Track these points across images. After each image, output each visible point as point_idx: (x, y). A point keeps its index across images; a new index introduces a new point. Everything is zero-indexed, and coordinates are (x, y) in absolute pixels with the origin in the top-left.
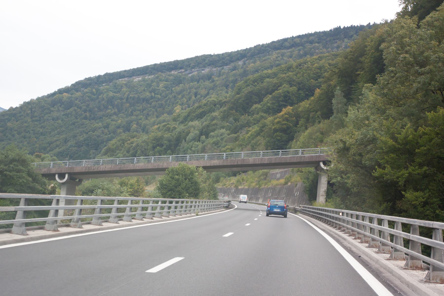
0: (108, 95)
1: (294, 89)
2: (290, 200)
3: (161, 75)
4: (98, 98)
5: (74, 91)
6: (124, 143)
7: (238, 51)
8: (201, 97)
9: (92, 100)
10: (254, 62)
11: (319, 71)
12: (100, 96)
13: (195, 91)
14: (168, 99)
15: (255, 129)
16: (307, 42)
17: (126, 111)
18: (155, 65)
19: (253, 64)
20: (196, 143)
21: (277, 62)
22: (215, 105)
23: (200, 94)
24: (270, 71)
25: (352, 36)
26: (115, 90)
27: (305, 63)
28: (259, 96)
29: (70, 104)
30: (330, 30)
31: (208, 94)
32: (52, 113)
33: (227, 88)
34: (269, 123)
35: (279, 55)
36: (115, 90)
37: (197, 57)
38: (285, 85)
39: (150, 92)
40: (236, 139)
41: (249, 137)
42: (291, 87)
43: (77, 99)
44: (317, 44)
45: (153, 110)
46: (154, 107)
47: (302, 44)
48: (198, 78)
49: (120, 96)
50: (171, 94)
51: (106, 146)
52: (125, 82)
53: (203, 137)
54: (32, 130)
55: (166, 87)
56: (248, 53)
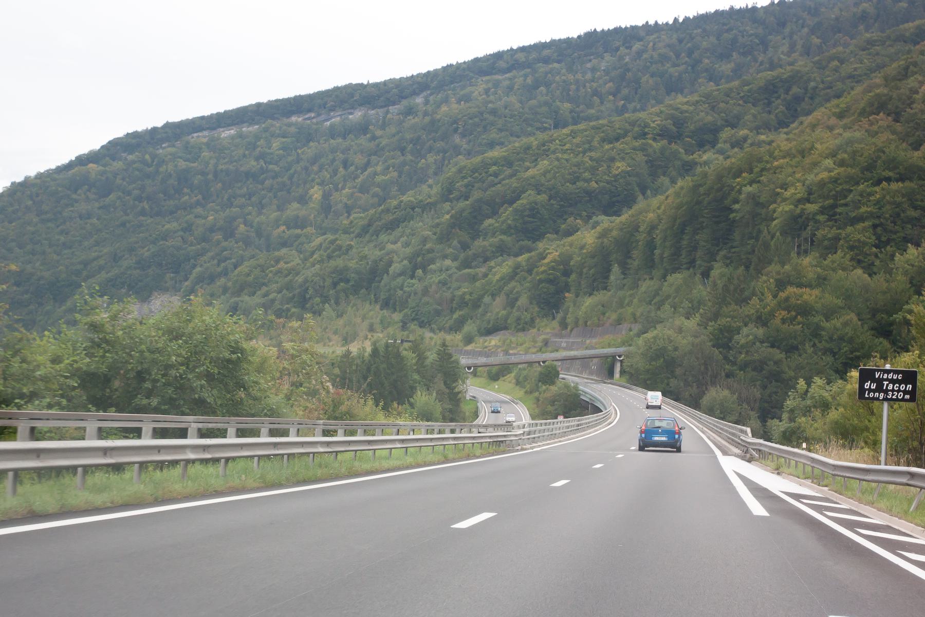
0: (176, 166)
1: (543, 198)
3: (272, 126)
5: (107, 158)
8: (357, 168)
11: (575, 169)
12: (161, 169)
18: (259, 105)
21: (490, 105)
22: (413, 209)
25: (617, 49)
26: (188, 156)
27: (552, 141)
30: (579, 37)
32: (76, 205)
34: (524, 264)
35: (490, 85)
36: (188, 156)
37: (336, 89)
38: (529, 192)
39: (257, 159)
41: (498, 281)
42: (539, 194)
44: (556, 65)
51: (194, 266)
52: (205, 140)
53: (419, 272)
55: (284, 148)
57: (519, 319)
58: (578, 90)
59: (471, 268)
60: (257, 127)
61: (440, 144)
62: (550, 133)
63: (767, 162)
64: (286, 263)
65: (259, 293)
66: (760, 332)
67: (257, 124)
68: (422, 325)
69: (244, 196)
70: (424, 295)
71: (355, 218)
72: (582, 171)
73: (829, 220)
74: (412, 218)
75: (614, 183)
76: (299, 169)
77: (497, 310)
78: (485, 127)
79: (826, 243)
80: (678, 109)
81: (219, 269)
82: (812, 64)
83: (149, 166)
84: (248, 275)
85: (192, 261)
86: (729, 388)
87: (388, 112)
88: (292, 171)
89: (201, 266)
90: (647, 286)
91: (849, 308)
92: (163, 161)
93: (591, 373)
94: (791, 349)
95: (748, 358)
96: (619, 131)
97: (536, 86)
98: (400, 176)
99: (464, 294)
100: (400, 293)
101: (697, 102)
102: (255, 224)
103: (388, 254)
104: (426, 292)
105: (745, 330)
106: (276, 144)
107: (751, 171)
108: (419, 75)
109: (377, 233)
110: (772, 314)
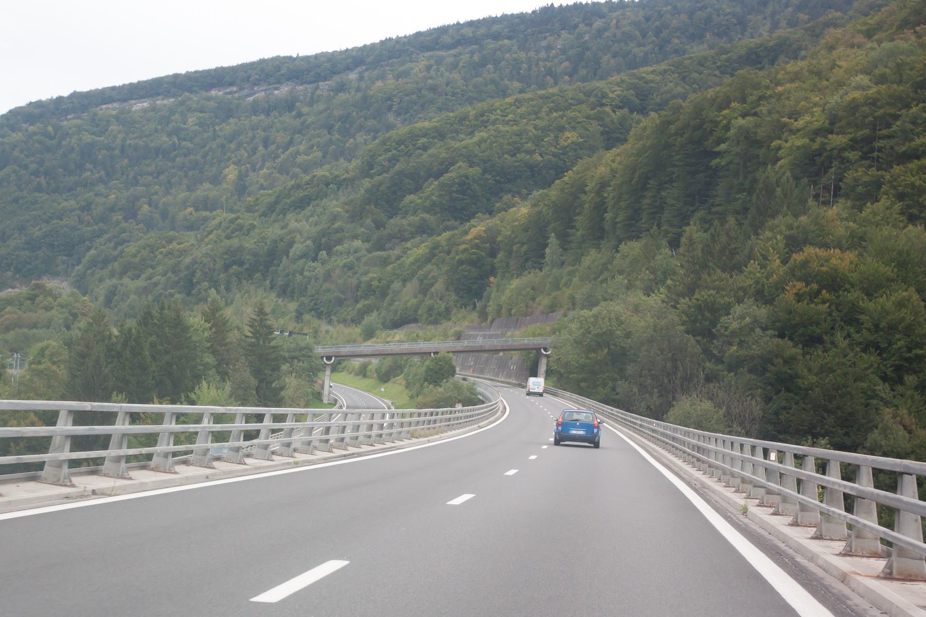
0: (80, 140)
1: (475, 171)
3: (189, 99)
5: (6, 129)
7: (347, 50)
8: (278, 147)
10: (382, 77)
12: (64, 143)
15: (418, 249)
17: (123, 174)
18: (176, 76)
19: (379, 84)
20: (311, 264)
21: (430, 81)
22: (327, 185)
23: (273, 143)
25: (576, 27)
26: (95, 129)
27: (491, 111)
28: (416, 180)
30: (534, 12)
31: (291, 143)
33: (330, 134)
34: (444, 243)
35: (432, 62)
36: (95, 129)
37: (262, 61)
38: (460, 163)
39: (170, 135)
41: (412, 264)
42: (470, 167)
43: (15, 146)
44: (506, 42)
47: (475, 41)
49: (106, 142)
50: (215, 140)
51: (89, 249)
52: (114, 113)
53: (323, 254)
55: (201, 124)
57: (431, 309)
58: (530, 69)
59: (385, 250)
61: (371, 123)
63: (767, 88)
64: (179, 244)
65: (143, 276)
66: (763, 312)
67: (173, 96)
68: (319, 316)
69: (151, 174)
70: (325, 281)
71: (262, 196)
73: (862, 158)
74: (326, 196)
75: (562, 157)
76: (215, 146)
77: (407, 298)
78: (423, 106)
79: (860, 189)
80: (641, 78)
81: (115, 253)
82: (803, 31)
83: (51, 138)
84: (135, 256)
85: (87, 243)
86: (711, 398)
87: (317, 88)
88: (207, 148)
90: (592, 258)
91: (904, 281)
92: (67, 134)
93: (509, 376)
94: (812, 341)
95: (743, 352)
96: (570, 101)
97: (483, 63)
98: (324, 157)
99: (372, 279)
100: (299, 278)
101: (665, 71)
102: (160, 205)
103: (290, 233)
104: (328, 276)
105: (738, 309)
106: (192, 120)
107: (743, 100)
108: (353, 49)
109: (284, 212)
110: (780, 287)
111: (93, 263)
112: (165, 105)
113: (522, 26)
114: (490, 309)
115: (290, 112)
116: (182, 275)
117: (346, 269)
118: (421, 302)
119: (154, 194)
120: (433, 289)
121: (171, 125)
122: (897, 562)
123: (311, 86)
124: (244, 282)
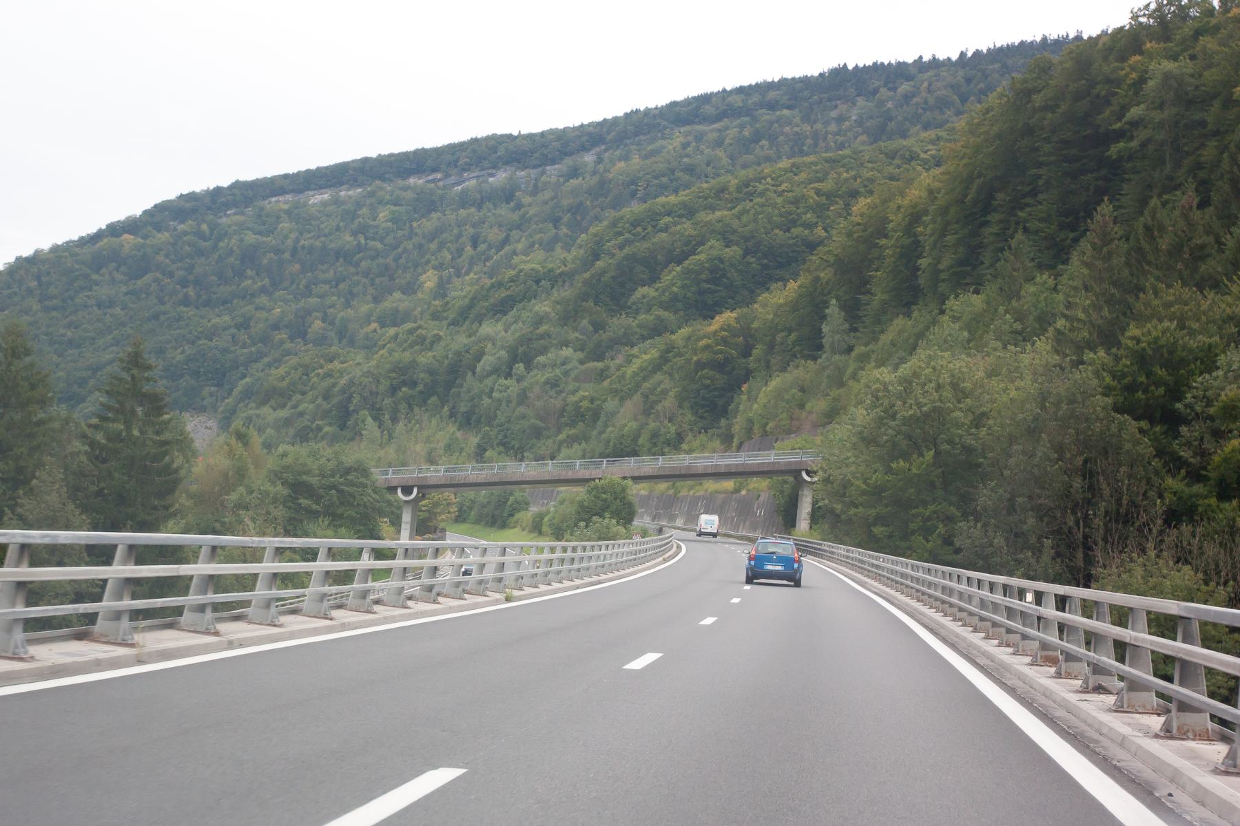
0: (242, 240)
1: (734, 252)
2: (748, 523)
3: (381, 188)
4: (215, 248)
5: (149, 228)
6: (307, 375)
7: (582, 125)
8: (490, 247)
9: (201, 253)
10: (626, 158)
11: (793, 208)
12: (221, 244)
13: (471, 231)
14: (403, 253)
15: (647, 354)
16: (762, 106)
17: (292, 283)
18: (365, 160)
19: (622, 164)
20: (502, 381)
22: (538, 282)
24: (672, 199)
25: (876, 91)
26: (262, 228)
27: (759, 180)
29: (140, 265)
30: (821, 75)
31: (506, 241)
32: (95, 288)
34: (681, 343)
35: (690, 138)
36: (262, 228)
37: (475, 141)
39: (354, 234)
40: (602, 375)
41: (635, 374)
42: (727, 246)
43: (160, 249)
44: (786, 112)
45: (364, 280)
46: (366, 274)
47: (746, 111)
48: (478, 196)
50: (411, 239)
51: (244, 376)
52: (286, 207)
53: (520, 367)
54: (47, 334)
55: (395, 220)
56: (609, 133)
57: (655, 435)
60: (359, 190)
62: (759, 169)
67: (359, 186)
70: (520, 403)
72: (801, 210)
76: (411, 246)
84: (283, 379)
87: (543, 173)
88: (400, 250)
89: (252, 375)
92: (226, 234)
97: (757, 137)
100: (486, 401)
104: (523, 398)
106: (383, 214)
108: (590, 124)
109: (480, 320)
111: (248, 394)
112: (350, 197)
113: (806, 93)
114: (736, 429)
115: (508, 203)
116: (335, 401)
117: (547, 387)
118: (642, 427)
119: (330, 307)
120: (659, 407)
121: (356, 222)
122: (1177, 718)
123: (535, 171)
124: (416, 410)
